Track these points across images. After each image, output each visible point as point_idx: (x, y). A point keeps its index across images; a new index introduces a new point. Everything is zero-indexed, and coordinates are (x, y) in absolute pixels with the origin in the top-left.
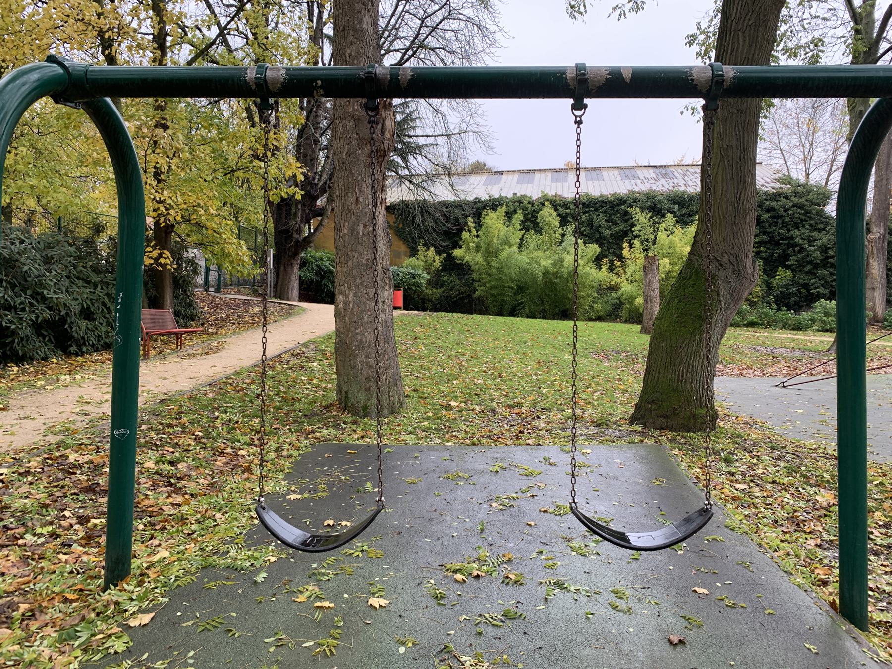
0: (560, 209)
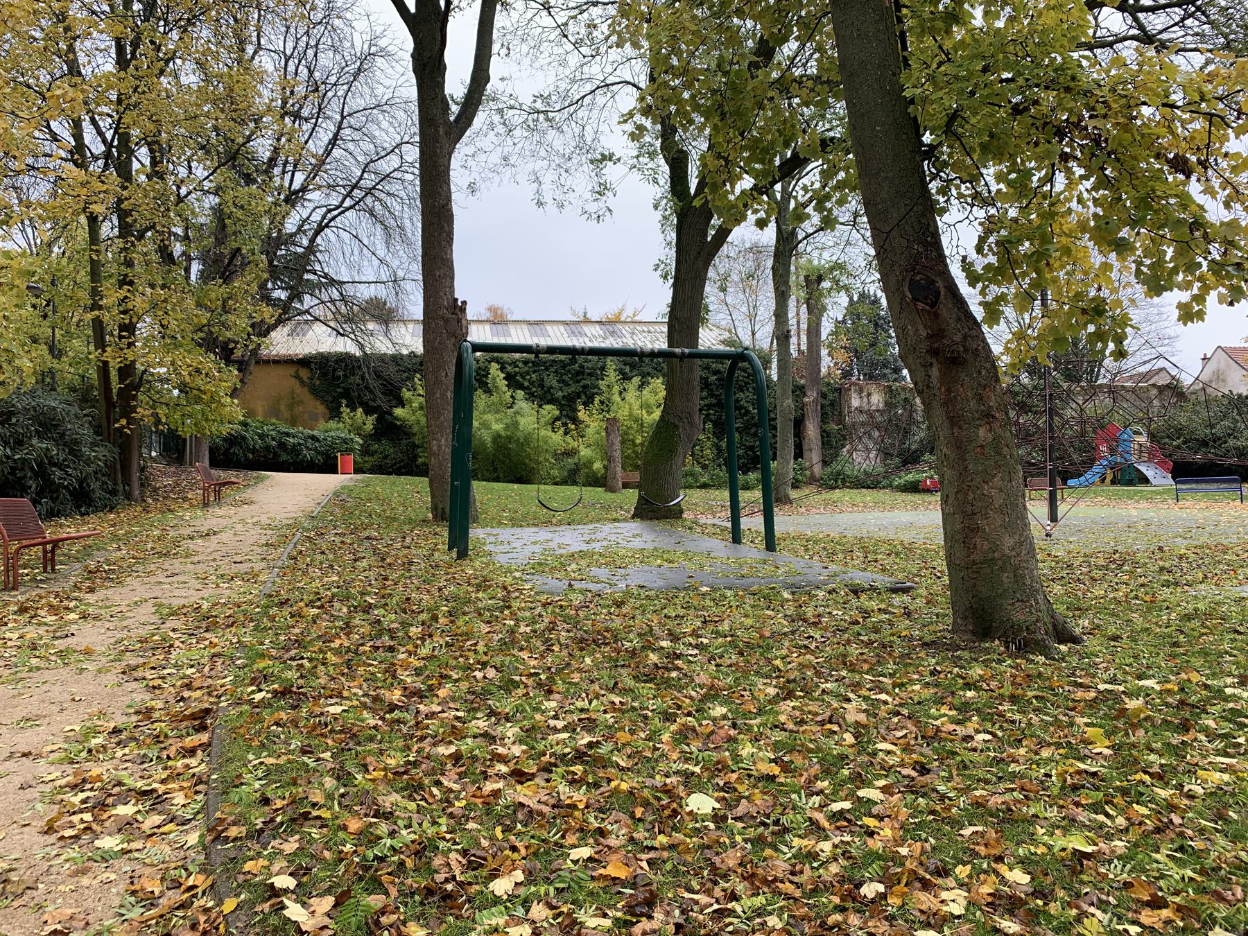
0: (509, 368)
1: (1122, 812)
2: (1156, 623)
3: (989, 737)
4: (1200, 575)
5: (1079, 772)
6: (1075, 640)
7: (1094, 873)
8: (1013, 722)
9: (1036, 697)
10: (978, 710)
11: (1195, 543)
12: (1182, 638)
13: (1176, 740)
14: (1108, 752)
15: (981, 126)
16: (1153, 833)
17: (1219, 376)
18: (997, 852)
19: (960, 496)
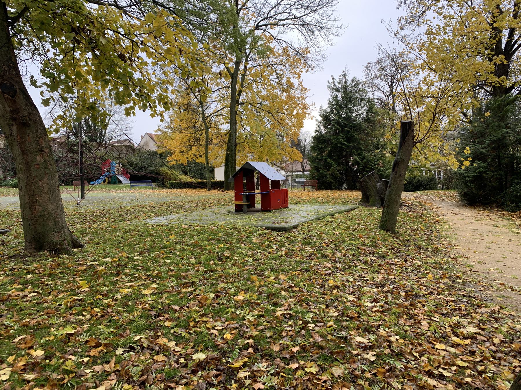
1: (89, 312)
2: (114, 236)
3: (36, 294)
4: (133, 217)
5: (74, 301)
6: (81, 246)
7: (74, 341)
8: (48, 285)
9: (60, 273)
10: (32, 283)
11: (133, 205)
12: (122, 240)
13: (113, 279)
14: (87, 290)
15: (36, 18)
16: (100, 318)
17: (146, 144)
18: (30, 345)
19: (28, 187)
